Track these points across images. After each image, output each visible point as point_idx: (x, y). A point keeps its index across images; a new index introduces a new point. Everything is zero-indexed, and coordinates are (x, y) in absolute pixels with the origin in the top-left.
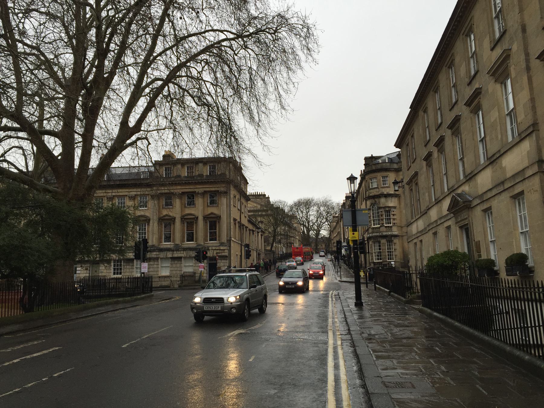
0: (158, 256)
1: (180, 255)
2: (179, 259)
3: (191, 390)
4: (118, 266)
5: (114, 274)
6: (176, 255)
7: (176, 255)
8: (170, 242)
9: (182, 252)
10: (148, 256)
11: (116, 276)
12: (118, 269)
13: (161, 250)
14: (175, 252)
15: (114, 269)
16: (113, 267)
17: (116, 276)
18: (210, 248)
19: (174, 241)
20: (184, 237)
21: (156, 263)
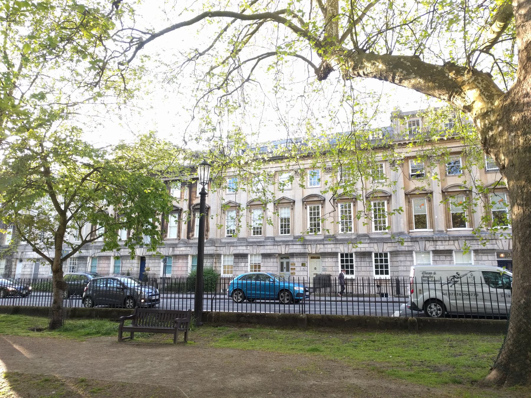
0: (410, 249)
1: (447, 248)
2: (449, 252)
3: (446, 97)
4: (347, 261)
5: (377, 273)
6: (441, 248)
7: (441, 246)
8: (426, 228)
9: (451, 242)
10: (196, 215)
11: (378, 277)
12: (382, 267)
13: (414, 240)
14: (439, 243)
15: (377, 267)
16: (374, 264)
17: (378, 277)
18: (417, 54)
19: (432, 226)
20: (449, 221)
21: (409, 258)
